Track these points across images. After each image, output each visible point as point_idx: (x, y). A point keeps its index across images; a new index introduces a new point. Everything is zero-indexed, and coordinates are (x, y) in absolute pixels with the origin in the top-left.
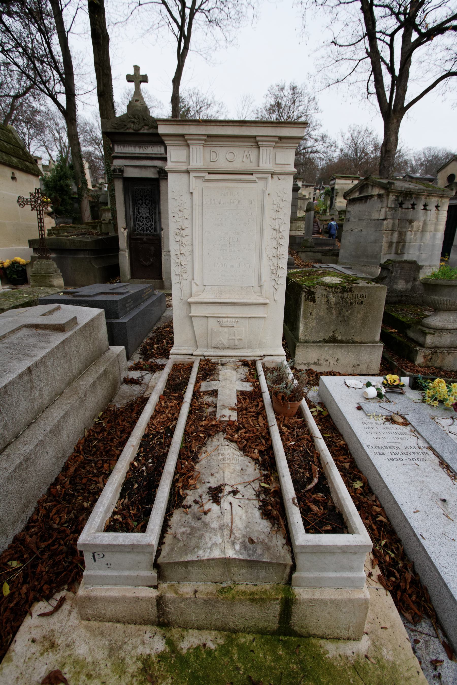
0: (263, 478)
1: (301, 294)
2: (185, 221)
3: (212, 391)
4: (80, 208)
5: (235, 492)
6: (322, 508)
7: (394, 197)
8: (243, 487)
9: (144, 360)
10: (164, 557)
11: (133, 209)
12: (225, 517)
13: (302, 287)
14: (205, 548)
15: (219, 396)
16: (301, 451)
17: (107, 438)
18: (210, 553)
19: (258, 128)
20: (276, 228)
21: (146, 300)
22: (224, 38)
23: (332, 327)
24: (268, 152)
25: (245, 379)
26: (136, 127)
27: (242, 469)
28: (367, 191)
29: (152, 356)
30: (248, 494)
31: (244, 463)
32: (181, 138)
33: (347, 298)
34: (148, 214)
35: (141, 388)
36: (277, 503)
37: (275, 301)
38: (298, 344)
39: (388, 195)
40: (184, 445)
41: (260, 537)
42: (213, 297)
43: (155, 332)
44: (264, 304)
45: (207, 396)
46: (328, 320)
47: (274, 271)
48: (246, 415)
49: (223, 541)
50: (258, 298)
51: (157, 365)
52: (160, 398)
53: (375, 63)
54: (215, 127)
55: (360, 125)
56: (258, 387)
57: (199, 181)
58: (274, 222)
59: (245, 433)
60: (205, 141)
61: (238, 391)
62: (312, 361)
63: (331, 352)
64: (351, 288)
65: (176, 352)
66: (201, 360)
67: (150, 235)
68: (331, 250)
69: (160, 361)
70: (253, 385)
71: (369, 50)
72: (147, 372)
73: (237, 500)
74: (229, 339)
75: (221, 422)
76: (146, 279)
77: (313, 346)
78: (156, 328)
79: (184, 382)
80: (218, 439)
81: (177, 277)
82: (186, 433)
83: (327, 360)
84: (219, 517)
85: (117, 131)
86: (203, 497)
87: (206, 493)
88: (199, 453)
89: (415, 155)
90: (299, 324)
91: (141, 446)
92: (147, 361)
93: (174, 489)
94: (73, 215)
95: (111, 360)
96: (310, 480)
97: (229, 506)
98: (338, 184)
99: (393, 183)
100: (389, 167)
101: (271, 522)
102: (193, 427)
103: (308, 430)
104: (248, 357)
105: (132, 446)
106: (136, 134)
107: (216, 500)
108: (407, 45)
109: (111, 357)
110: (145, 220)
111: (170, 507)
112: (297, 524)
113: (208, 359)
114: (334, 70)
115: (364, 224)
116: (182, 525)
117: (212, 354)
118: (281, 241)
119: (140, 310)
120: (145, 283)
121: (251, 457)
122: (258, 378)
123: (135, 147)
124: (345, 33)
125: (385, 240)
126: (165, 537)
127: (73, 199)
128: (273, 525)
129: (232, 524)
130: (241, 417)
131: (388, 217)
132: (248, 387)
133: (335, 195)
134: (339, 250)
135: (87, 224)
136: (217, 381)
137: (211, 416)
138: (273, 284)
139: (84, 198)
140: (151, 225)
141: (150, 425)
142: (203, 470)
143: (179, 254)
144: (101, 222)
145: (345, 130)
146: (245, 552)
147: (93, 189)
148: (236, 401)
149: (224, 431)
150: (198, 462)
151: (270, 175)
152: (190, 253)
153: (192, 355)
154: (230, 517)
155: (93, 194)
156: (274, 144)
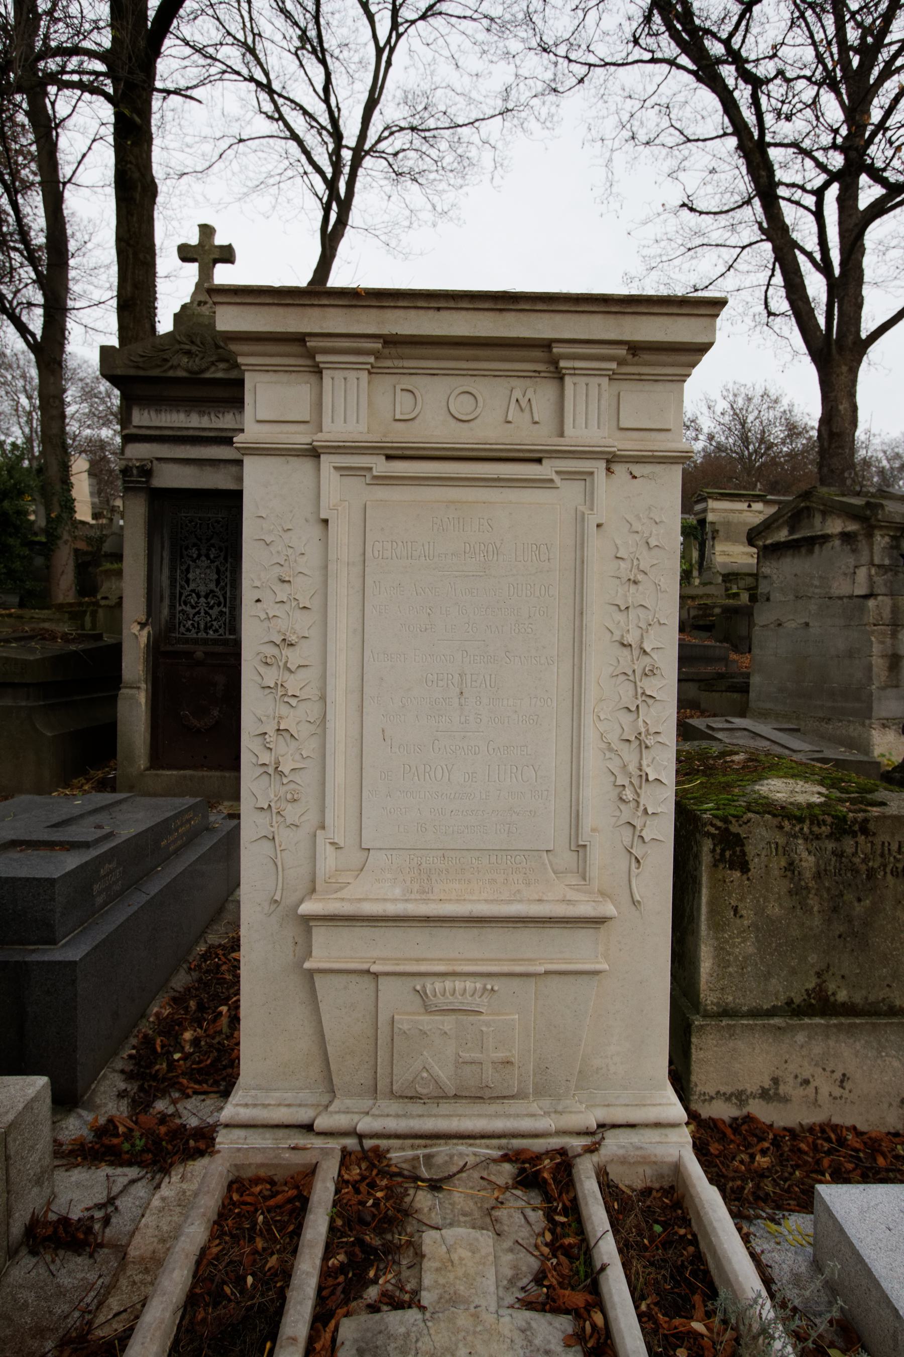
1: (699, 844)
2: (299, 614)
4: (48, 567)
7: (887, 539)
11: (173, 569)
13: (699, 819)
19: (558, 318)
20: (630, 639)
22: (429, 207)
23: (813, 958)
24: (594, 391)
26: (195, 364)
28: (812, 526)
29: (164, 1085)
32: (295, 348)
33: (855, 854)
34: (212, 586)
35: (92, 1276)
37: (635, 903)
38: (698, 1021)
39: (870, 536)
42: (397, 892)
44: (598, 922)
47: (629, 794)
50: (572, 895)
53: (781, 249)
54: (412, 313)
55: (749, 385)
57: (356, 483)
58: (620, 617)
60: (378, 355)
62: (752, 1087)
63: (817, 1048)
64: (866, 820)
65: (245, 1114)
66: (346, 1154)
67: (215, 642)
68: (721, 676)
69: (193, 1112)
71: (765, 225)
72: (133, 1172)
74: (460, 1063)
76: (195, 767)
77: (751, 1028)
78: (202, 948)
81: (262, 819)
83: (806, 1082)
85: (141, 373)
89: (885, 448)
90: (697, 946)
94: (28, 585)
98: (713, 510)
99: (882, 506)
100: (843, 472)
106: (195, 380)
108: (850, 216)
110: (202, 600)
113: (375, 1149)
114: (686, 266)
115: (813, 608)
117: (392, 1125)
118: (651, 686)
119: (144, 898)
122: (591, 1281)
123: (188, 413)
124: (709, 189)
125: (876, 649)
127: (31, 544)
131: (877, 591)
133: (710, 535)
134: (748, 676)
135: (60, 607)
136: (412, 1315)
138: (627, 841)
139: (60, 542)
140: (222, 613)
143: (271, 732)
144: (96, 604)
145: (716, 395)
147: (94, 522)
151: (603, 465)
152: (312, 728)
155: (92, 533)
156: (614, 365)
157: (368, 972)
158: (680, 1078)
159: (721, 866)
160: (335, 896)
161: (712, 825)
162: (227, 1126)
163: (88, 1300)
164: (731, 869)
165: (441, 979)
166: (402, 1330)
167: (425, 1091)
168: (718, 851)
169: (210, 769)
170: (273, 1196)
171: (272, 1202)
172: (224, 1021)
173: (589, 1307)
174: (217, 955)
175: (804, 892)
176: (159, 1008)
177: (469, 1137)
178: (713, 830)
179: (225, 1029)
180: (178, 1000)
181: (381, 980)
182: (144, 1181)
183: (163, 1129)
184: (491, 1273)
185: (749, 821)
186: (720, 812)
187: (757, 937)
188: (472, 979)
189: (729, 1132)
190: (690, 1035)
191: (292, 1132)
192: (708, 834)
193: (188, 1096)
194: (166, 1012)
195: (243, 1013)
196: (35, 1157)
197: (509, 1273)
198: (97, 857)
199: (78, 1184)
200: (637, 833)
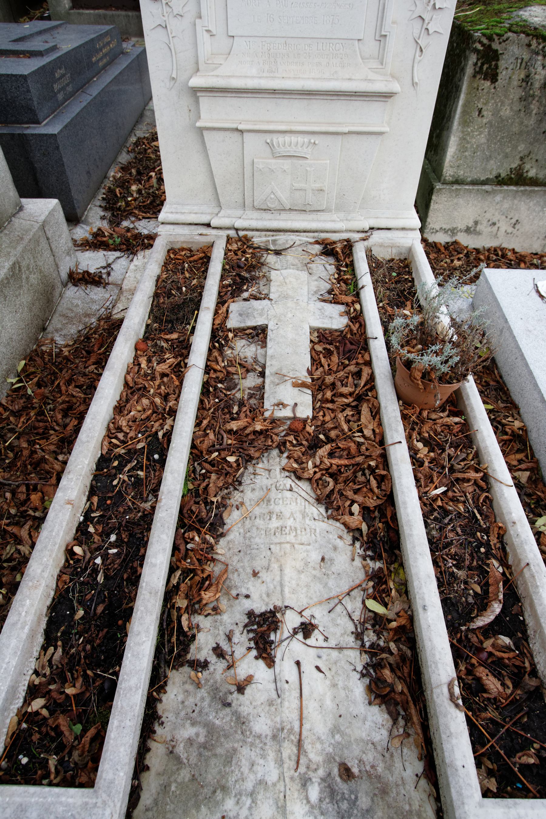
0: (371, 584)
1: (466, 59)
3: (254, 328)
5: (307, 629)
6: (509, 683)
8: (325, 612)
9: (111, 222)
10: (147, 810)
12: (286, 704)
13: (470, 37)
14: (241, 794)
15: (269, 344)
16: (459, 515)
17: (35, 428)
18: (250, 808)
21: (104, 67)
25: (330, 292)
27: (323, 559)
29: (127, 213)
30: (338, 631)
31: (329, 542)
35: (107, 296)
36: (403, 657)
37: (414, 84)
38: (438, 186)
40: (191, 486)
41: (365, 758)
42: (254, 71)
43: (133, 150)
44: (387, 96)
45: (243, 342)
46: (516, 129)
48: (332, 401)
49: (281, 777)
50: (372, 76)
51: (138, 236)
52: (136, 349)
56: (357, 318)
59: (331, 455)
61: (313, 330)
62: (461, 226)
65: (172, 218)
66: (229, 240)
69: (144, 227)
70: (348, 313)
72: (118, 254)
73: (313, 652)
75: (274, 421)
77: (470, 191)
78: (133, 139)
79: (191, 300)
80: (270, 471)
82: (196, 454)
83: (494, 224)
84: (271, 703)
86: (235, 639)
87: (241, 625)
88: (225, 506)
90: (448, 137)
91: (92, 492)
92: (118, 224)
93: (169, 615)
95: (27, 238)
96: (482, 603)
97: (295, 668)
101: (390, 713)
102: (212, 436)
103: (477, 455)
104: (335, 232)
105: (69, 502)
107: (264, 650)
109: (27, 231)
111: (158, 664)
112: (461, 771)
113: (245, 237)
116: (188, 717)
119: (89, 98)
120: (98, 21)
121: (345, 524)
126: (149, 750)
128: (395, 722)
129: (301, 725)
130: (321, 408)
132: (334, 319)
136: (266, 302)
137: (253, 401)
141: (112, 431)
142: (236, 559)
146: (330, 807)
148: (307, 362)
149: (282, 446)
150: (222, 535)
153: (208, 225)
154: (296, 703)
157: (237, 130)
158: (423, 205)
159: (478, 77)
160: (212, 73)
161: (480, 42)
162: (163, 223)
163: (108, 304)
164: (484, 79)
165: (282, 135)
166: (261, 307)
167: (273, 206)
168: (479, 64)
169: (117, 8)
170: (191, 256)
171: (191, 259)
172: (154, 181)
173: (353, 303)
174: (144, 143)
175: (530, 99)
176: (114, 173)
177: (297, 231)
178: (479, 47)
179: (155, 185)
180: (125, 169)
181: (245, 134)
182: (124, 258)
183: (129, 234)
184: (306, 289)
185: (507, 39)
186: (488, 32)
187: (489, 131)
188: (302, 136)
189: (442, 249)
190: (432, 194)
191: (199, 227)
192: (476, 51)
193: (140, 220)
194: (119, 175)
195: (165, 176)
196: (63, 241)
197: (315, 289)
198: (50, 62)
199: (90, 258)
200: (425, 26)
